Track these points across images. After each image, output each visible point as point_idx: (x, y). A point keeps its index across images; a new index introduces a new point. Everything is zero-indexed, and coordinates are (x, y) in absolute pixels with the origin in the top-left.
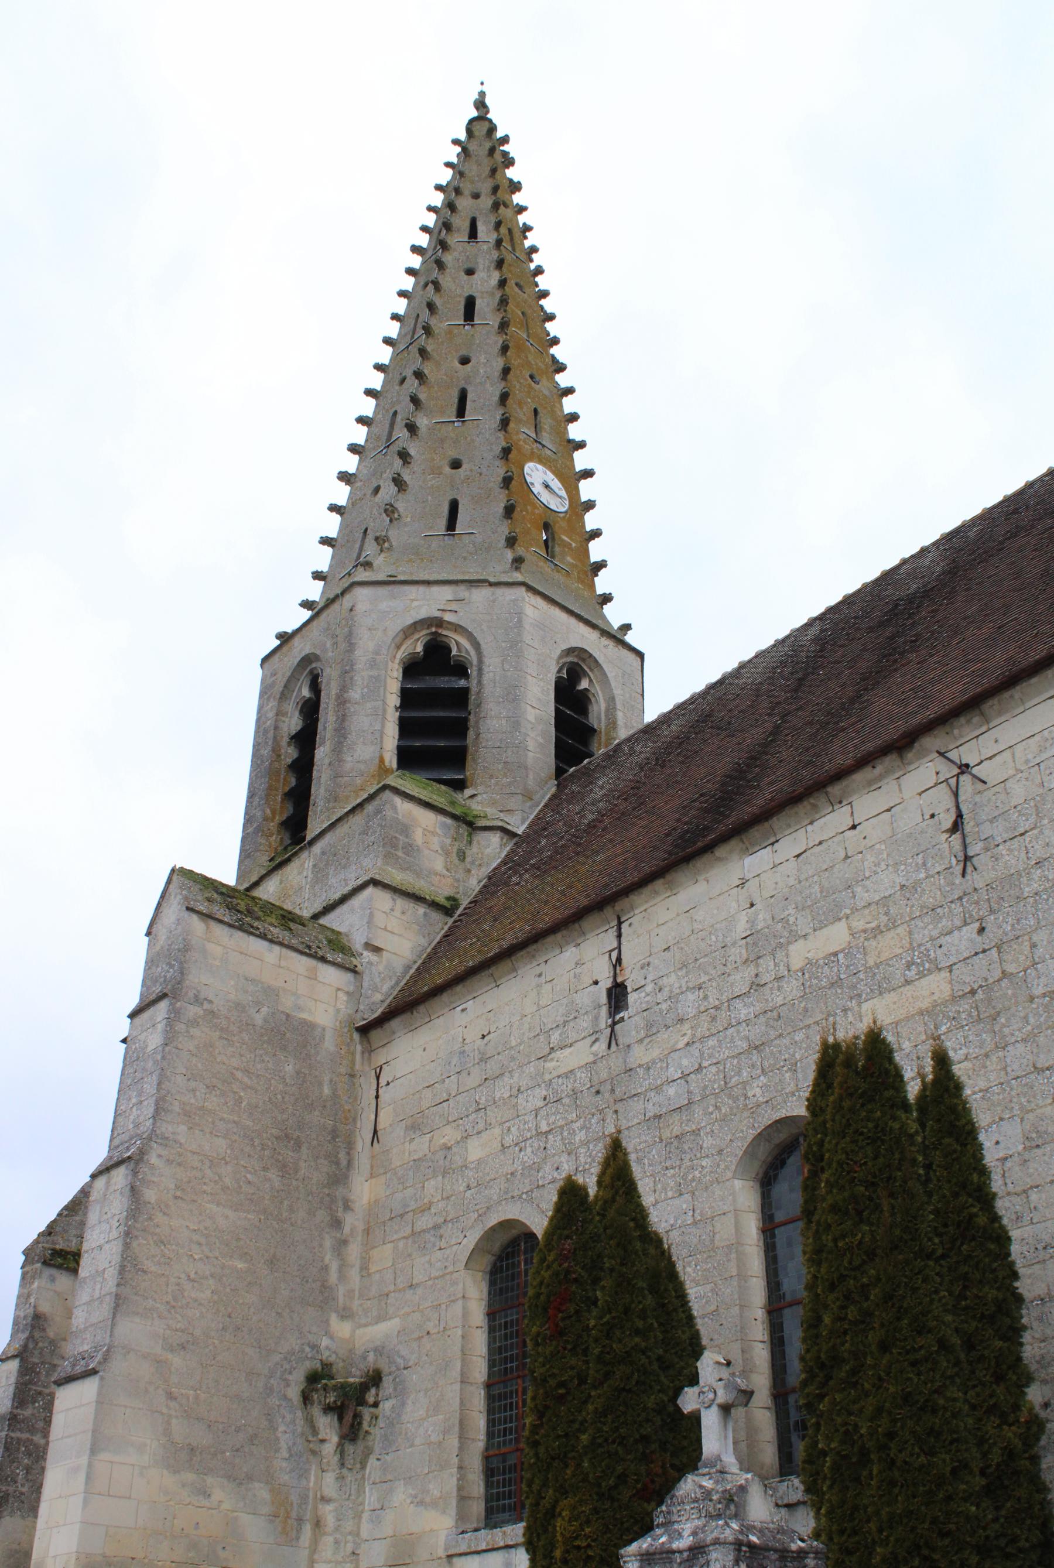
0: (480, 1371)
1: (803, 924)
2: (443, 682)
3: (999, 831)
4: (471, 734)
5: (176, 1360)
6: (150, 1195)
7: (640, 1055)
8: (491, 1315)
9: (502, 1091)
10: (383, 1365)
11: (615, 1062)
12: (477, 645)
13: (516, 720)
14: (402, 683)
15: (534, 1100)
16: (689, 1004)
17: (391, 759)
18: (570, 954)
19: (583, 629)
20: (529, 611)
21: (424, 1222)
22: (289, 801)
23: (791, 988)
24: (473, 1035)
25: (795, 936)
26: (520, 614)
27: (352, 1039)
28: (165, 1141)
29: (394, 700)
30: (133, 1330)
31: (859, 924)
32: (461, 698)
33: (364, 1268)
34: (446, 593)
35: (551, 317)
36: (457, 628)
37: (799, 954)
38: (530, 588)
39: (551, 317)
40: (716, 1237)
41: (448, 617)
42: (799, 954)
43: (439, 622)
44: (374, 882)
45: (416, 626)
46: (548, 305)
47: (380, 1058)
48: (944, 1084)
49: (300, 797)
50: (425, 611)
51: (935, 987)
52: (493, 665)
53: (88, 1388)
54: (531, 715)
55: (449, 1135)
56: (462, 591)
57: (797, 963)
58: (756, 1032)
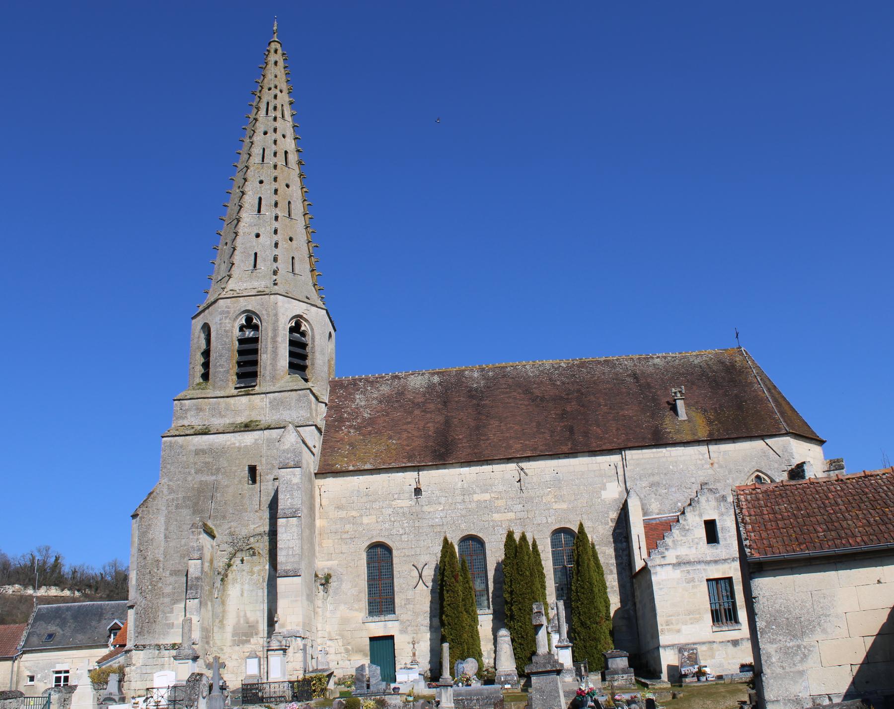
1: (478, 490)
3: (529, 486)
7: (426, 508)
10: (330, 572)
11: (418, 508)
12: (312, 329)
16: (443, 500)
23: (474, 505)
25: (475, 493)
27: (768, 624)
31: (493, 495)
36: (306, 320)
37: (476, 497)
40: (495, 554)
41: (305, 316)
42: (476, 497)
44: (316, 426)
48: (535, 545)
51: (511, 515)
57: (475, 500)
58: (464, 512)
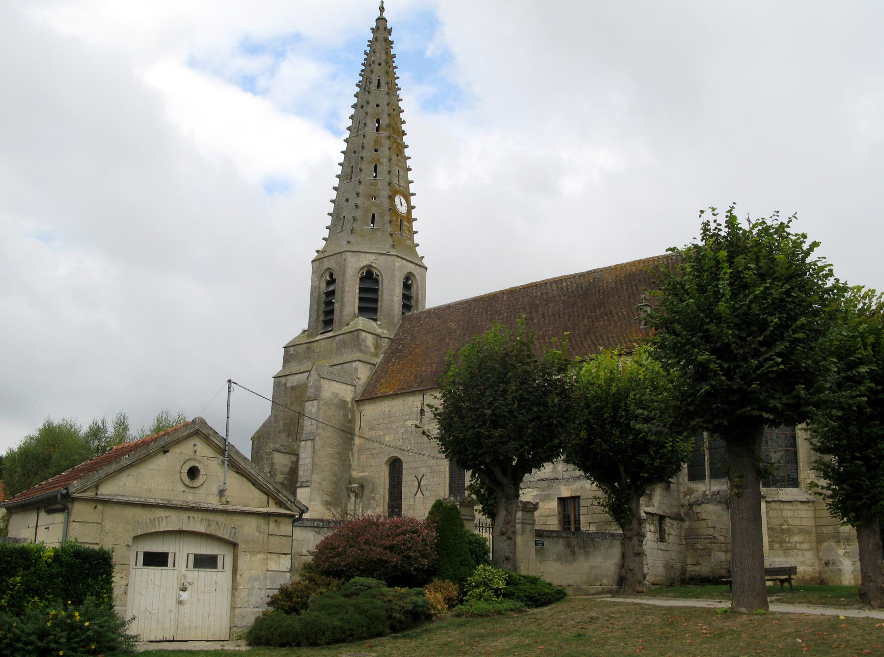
0: (387, 487)
2: (372, 286)
4: (379, 303)
5: (323, 483)
6: (317, 447)
8: (390, 475)
9: (394, 426)
13: (391, 296)
14: (360, 284)
15: (402, 430)
17: (357, 311)
18: (411, 398)
19: (411, 265)
20: (397, 264)
21: (374, 452)
22: (325, 309)
24: (387, 410)
26: (394, 265)
28: (319, 435)
29: (358, 291)
30: (316, 478)
32: (376, 291)
33: (358, 459)
34: (373, 257)
35: (404, 122)
38: (397, 256)
39: (404, 122)
43: (371, 266)
45: (363, 267)
46: (409, 163)
47: (361, 408)
49: (329, 312)
50: (366, 262)
52: (386, 282)
53: (307, 490)
54: (396, 299)
55: (380, 433)
56: (377, 256)
